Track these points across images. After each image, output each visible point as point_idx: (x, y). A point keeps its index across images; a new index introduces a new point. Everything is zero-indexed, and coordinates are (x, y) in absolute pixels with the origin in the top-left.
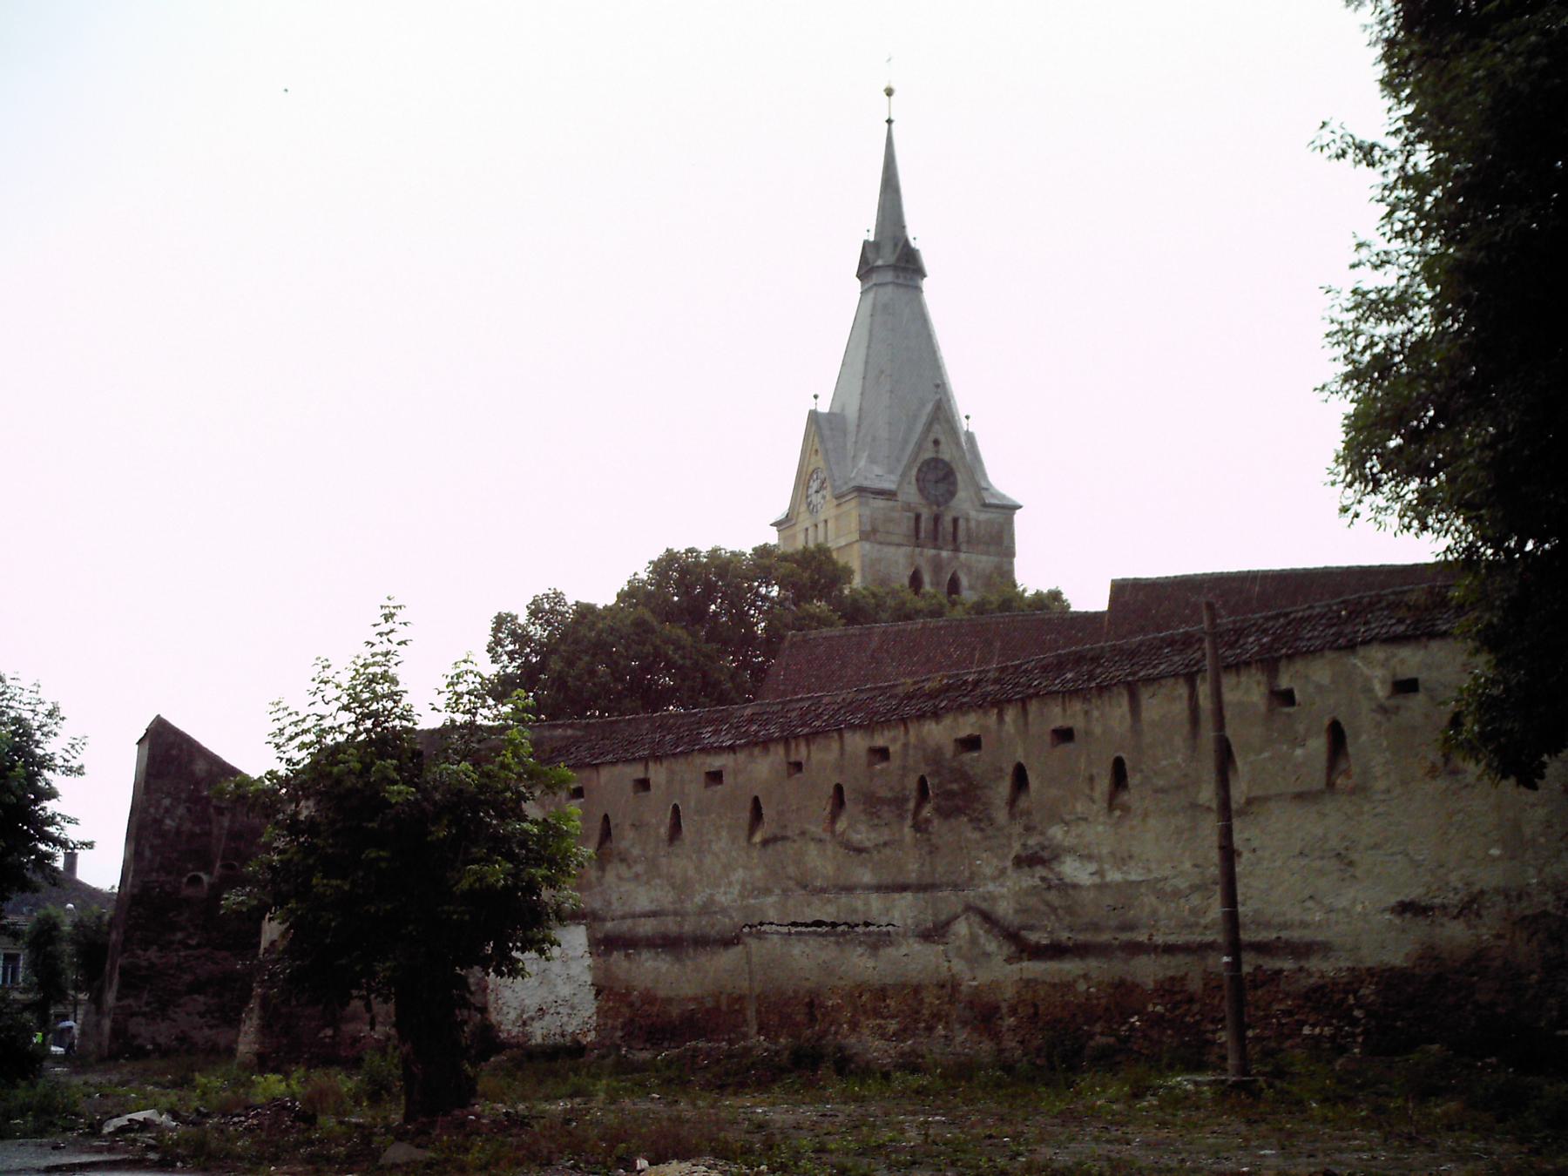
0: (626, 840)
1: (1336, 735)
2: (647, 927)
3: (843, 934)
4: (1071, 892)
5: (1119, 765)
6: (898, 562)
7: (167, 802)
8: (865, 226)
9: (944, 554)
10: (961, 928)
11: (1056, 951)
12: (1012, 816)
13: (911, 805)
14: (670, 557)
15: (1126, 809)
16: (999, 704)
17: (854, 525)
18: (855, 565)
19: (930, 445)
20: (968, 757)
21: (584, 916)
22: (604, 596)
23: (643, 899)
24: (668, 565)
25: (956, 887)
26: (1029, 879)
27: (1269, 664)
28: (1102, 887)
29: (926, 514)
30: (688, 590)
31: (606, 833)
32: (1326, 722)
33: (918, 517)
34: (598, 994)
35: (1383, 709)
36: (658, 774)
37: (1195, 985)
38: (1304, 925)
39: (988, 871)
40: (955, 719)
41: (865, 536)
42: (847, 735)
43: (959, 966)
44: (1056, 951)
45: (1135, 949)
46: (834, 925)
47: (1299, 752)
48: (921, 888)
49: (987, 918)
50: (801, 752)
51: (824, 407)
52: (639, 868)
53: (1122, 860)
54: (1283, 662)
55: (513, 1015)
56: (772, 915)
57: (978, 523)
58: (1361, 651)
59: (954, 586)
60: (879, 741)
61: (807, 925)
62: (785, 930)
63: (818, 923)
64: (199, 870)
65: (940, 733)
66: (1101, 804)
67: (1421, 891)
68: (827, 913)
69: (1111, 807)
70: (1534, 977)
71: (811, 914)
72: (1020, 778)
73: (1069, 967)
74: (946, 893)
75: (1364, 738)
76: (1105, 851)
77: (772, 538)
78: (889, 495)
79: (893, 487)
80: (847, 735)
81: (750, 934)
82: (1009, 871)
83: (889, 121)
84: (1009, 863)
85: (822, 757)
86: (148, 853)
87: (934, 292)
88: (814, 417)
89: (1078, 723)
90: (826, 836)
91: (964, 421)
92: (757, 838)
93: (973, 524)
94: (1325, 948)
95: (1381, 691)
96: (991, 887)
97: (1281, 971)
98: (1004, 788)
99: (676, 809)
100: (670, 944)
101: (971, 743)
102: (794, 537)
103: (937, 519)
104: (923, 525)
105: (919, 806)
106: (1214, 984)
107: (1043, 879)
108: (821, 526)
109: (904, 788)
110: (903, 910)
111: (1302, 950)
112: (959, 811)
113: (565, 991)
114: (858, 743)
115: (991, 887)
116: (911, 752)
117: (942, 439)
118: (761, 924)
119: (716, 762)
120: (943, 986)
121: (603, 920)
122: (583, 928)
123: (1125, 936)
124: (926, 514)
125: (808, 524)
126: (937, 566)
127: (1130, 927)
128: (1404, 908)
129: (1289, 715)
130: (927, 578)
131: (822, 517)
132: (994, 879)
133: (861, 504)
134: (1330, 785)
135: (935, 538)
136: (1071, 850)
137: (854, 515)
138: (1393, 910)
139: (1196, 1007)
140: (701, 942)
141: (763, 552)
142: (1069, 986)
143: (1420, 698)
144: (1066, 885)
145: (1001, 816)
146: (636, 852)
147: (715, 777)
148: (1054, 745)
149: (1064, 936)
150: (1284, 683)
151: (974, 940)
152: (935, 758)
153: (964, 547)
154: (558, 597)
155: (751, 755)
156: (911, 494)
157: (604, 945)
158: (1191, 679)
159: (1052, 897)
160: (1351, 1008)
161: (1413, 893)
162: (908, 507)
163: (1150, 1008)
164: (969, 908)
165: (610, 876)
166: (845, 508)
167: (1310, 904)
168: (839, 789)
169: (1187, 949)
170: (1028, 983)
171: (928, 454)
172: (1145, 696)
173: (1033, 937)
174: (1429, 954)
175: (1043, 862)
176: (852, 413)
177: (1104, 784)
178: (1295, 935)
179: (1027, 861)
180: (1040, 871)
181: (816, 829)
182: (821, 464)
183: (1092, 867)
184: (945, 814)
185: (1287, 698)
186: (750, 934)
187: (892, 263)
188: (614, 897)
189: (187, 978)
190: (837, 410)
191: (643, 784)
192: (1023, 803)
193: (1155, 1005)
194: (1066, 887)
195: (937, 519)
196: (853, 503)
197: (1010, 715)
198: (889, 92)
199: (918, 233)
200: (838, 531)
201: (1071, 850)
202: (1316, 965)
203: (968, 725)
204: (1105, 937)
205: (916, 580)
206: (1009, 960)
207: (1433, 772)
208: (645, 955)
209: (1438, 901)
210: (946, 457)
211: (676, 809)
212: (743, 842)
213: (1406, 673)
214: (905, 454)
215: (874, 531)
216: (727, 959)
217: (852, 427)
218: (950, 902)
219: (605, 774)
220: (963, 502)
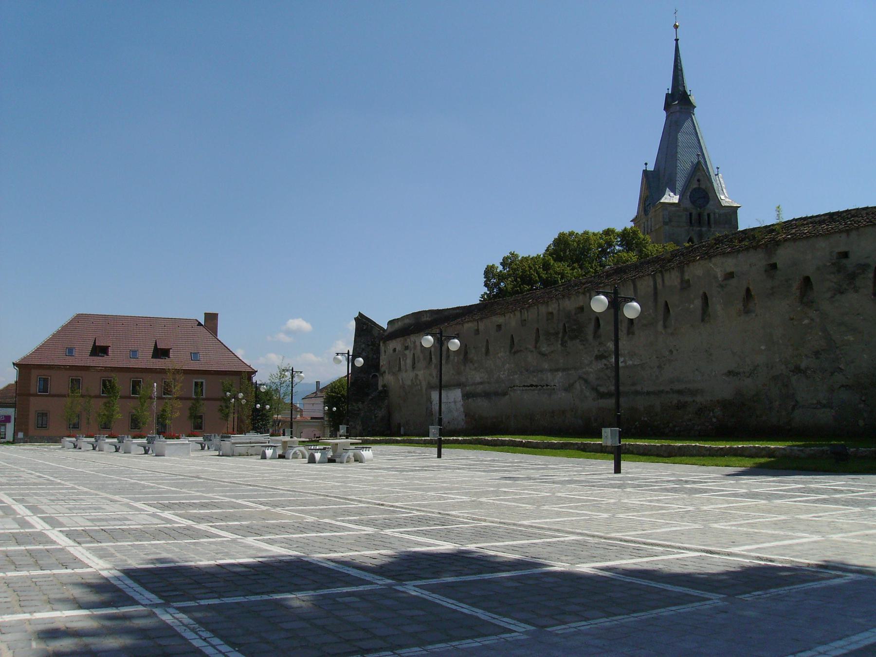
1: (705, 298)
2: (480, 389)
7: (363, 346)
8: (666, 85)
9: (704, 229)
10: (577, 385)
13: (560, 335)
19: (696, 181)
23: (478, 377)
29: (694, 212)
32: (701, 292)
33: (691, 214)
35: (721, 286)
39: (586, 361)
45: (637, 393)
46: (537, 386)
48: (564, 370)
49: (586, 381)
51: (651, 167)
52: (476, 365)
56: (517, 382)
57: (720, 215)
58: (713, 260)
60: (550, 310)
63: (532, 386)
68: (534, 381)
70: (777, 403)
71: (529, 382)
83: (677, 40)
87: (699, 116)
88: (645, 173)
93: (717, 215)
97: (686, 402)
98: (591, 328)
99: (487, 341)
100: (487, 395)
103: (700, 215)
104: (693, 218)
110: (558, 379)
111: (693, 393)
113: (456, 414)
114: (543, 309)
117: (701, 178)
124: (694, 212)
125: (644, 220)
127: (634, 384)
128: (730, 373)
135: (700, 223)
145: (590, 337)
146: (475, 358)
153: (713, 226)
157: (466, 396)
158: (654, 277)
162: (686, 210)
164: (580, 378)
168: (538, 329)
169: (654, 393)
171: (695, 185)
172: (639, 284)
173: (602, 389)
180: (604, 361)
181: (530, 347)
187: (679, 102)
195: (700, 215)
198: (676, 27)
202: (699, 399)
209: (742, 370)
210: (703, 187)
211: (487, 341)
213: (729, 270)
215: (670, 221)
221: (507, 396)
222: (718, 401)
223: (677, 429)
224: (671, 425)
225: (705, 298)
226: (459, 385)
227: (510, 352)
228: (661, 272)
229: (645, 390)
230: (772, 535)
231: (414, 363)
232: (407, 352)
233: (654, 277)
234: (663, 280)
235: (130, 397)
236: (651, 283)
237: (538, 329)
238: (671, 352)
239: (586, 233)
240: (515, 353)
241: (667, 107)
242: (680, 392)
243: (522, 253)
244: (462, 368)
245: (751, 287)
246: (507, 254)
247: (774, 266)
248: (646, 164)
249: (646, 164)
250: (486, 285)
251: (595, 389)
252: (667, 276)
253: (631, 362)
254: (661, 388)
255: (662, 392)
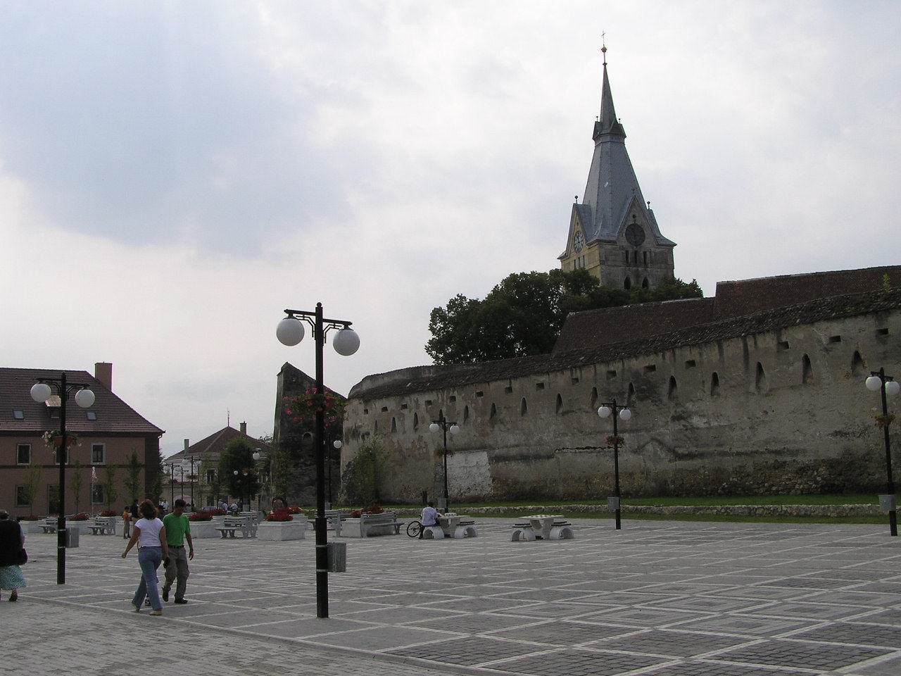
0: (503, 414)
1: (807, 361)
2: (514, 451)
3: (599, 452)
4: (696, 430)
5: (715, 375)
6: (619, 274)
8: (594, 112)
10: (650, 448)
11: (691, 456)
12: (670, 398)
13: (626, 395)
14: (513, 276)
15: (719, 395)
16: (663, 350)
17: (597, 258)
18: (599, 276)
20: (649, 374)
21: (486, 448)
22: (482, 297)
23: (511, 439)
24: (514, 282)
25: (647, 430)
26: (678, 426)
27: (778, 330)
28: (709, 428)
29: (631, 251)
30: (521, 293)
31: (494, 412)
33: (627, 252)
34: (493, 480)
35: (827, 350)
36: (516, 385)
37: (750, 469)
38: (794, 442)
40: (644, 358)
41: (602, 263)
42: (597, 366)
43: (649, 464)
44: (691, 456)
45: (724, 454)
46: (595, 448)
47: (791, 368)
49: (660, 443)
50: (577, 374)
51: (580, 202)
52: (509, 426)
53: (718, 416)
54: (783, 331)
55: (456, 491)
57: (656, 254)
58: (816, 324)
59: (645, 283)
60: (612, 369)
61: (583, 449)
62: (573, 451)
63: (588, 448)
64: (309, 430)
65: (638, 364)
66: (709, 393)
67: (844, 426)
69: (712, 395)
72: (673, 382)
73: (697, 463)
74: (642, 433)
75: (818, 361)
76: (710, 413)
77: (558, 265)
78: (613, 243)
79: (614, 239)
80: (597, 366)
81: (558, 453)
82: (669, 423)
83: (605, 64)
84: (669, 420)
85: (587, 374)
86: (286, 424)
87: (631, 145)
88: (575, 206)
89: (697, 359)
90: (590, 410)
91: (647, 205)
92: (561, 411)
94: (804, 451)
95: (825, 341)
96: (662, 430)
98: (666, 387)
99: (524, 401)
100: (524, 458)
101: (652, 368)
102: (569, 263)
103: (636, 253)
105: (630, 396)
106: (757, 468)
107: (684, 426)
108: (581, 258)
109: (623, 388)
112: (647, 398)
113: (479, 480)
114: (602, 369)
115: (662, 430)
116: (626, 373)
117: (637, 215)
118: (563, 449)
119: (542, 379)
120: (643, 473)
121: (494, 449)
122: (486, 453)
123: (719, 449)
124: (631, 251)
125: (574, 258)
126: (637, 275)
127: (720, 445)
128: (837, 433)
129: (786, 353)
130: (632, 281)
131: (582, 254)
132: (663, 426)
133: (600, 247)
134: (804, 382)
136: (696, 413)
137: (597, 252)
138: (832, 435)
139: (750, 478)
140: (537, 457)
141: (555, 273)
142: (696, 471)
143: (842, 343)
144: (694, 428)
145: (665, 399)
146: (508, 419)
147: (541, 386)
148: (687, 368)
149: (694, 449)
150: (784, 340)
151: (655, 453)
152: (636, 374)
154: (462, 298)
155: (556, 375)
156: (623, 242)
157: (495, 459)
158: (744, 339)
159: (688, 433)
160: (815, 477)
161: (840, 427)
163: (731, 479)
164: (652, 439)
165: (496, 428)
166: (593, 249)
167: (797, 433)
168: (595, 389)
170: (679, 471)
173: (680, 451)
174: (847, 452)
175: (684, 419)
176: (593, 205)
177: (709, 384)
178: (790, 446)
179: (677, 418)
180: (683, 422)
182: (580, 229)
183: (705, 420)
184: (642, 399)
185: (786, 345)
186: (558, 453)
187: (609, 132)
188: (499, 439)
189: (307, 479)
190: (587, 204)
191: (510, 390)
192: (675, 393)
193: (733, 478)
194: (694, 429)
195: (636, 253)
196: (596, 247)
197: (668, 355)
198: (604, 50)
199: (621, 115)
200: (591, 262)
201: (696, 413)
202: (800, 458)
203: (652, 360)
204: (711, 449)
205: (627, 282)
206: (670, 461)
207: (847, 376)
208: (513, 463)
211: (524, 401)
212: (554, 414)
213: (835, 334)
214: (617, 216)
215: (607, 259)
216: (549, 464)
217: (594, 211)
218: (645, 436)
219: (493, 385)
220: (648, 244)
221: (553, 460)
222: (823, 461)
223: (774, 489)
224: (766, 484)
225: (807, 361)
226: (483, 448)
227: (557, 412)
228: (754, 334)
229: (734, 450)
230: (613, 647)
231: (416, 422)
232: (406, 412)
233: (744, 339)
234: (755, 343)
235: (16, 467)
236: (741, 345)
237: (595, 389)
238: (766, 412)
239: (533, 273)
240: (564, 414)
241: (596, 137)
242: (778, 452)
243: (470, 296)
244: (489, 429)
245: (860, 352)
246: (454, 296)
247: (885, 332)
248: (576, 197)
249: (576, 197)
250: (432, 329)
251: (672, 450)
252: (760, 339)
253: (716, 424)
254: (755, 449)
255: (756, 452)
